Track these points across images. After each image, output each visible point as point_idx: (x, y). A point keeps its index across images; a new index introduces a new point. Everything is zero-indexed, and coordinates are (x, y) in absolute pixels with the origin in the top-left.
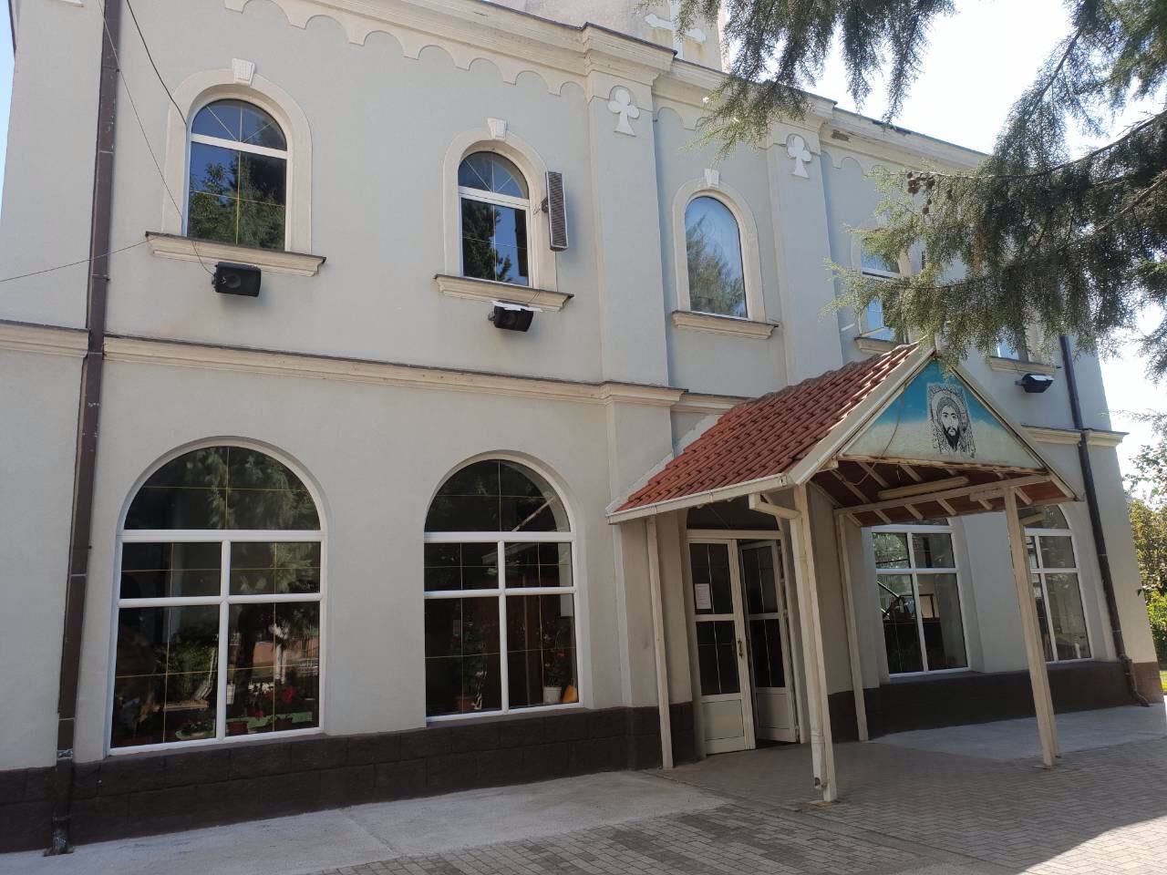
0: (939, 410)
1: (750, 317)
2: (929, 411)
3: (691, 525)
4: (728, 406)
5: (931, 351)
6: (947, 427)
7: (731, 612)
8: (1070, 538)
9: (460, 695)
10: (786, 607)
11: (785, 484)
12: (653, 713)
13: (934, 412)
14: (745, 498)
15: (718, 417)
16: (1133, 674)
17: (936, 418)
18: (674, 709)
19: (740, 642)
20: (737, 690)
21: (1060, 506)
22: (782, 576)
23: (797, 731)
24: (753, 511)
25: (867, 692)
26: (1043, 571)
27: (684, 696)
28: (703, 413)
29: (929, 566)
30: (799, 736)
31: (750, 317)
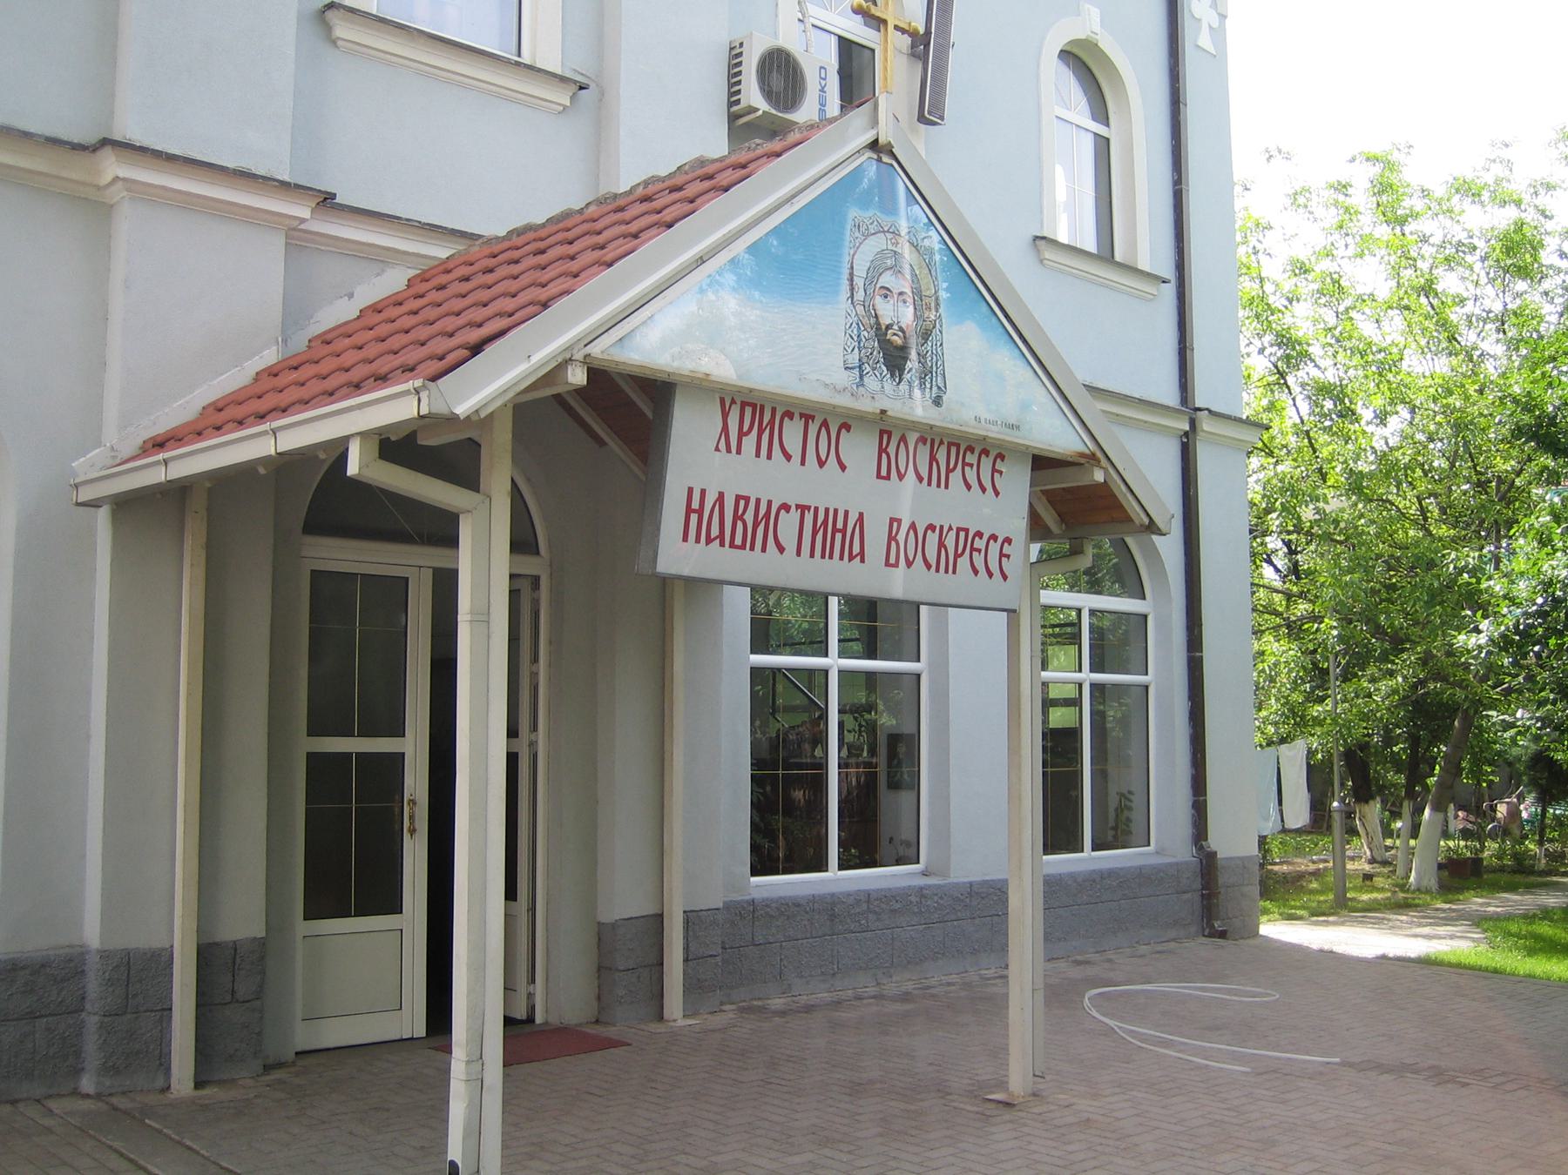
0: (871, 280)
1: (1187, 428)
2: (846, 276)
3: (316, 525)
4: (441, 251)
5: (869, 137)
6: (885, 321)
7: (401, 733)
8: (1145, 617)
9: (777, 813)
10: (534, 728)
11: (425, 411)
12: (160, 962)
13: (859, 282)
14: (339, 449)
15: (412, 273)
16: (1222, 879)
17: (860, 295)
18: (207, 955)
19: (413, 802)
20: (395, 907)
21: (1129, 540)
22: (535, 660)
23: (530, 996)
24: (355, 483)
25: (691, 918)
26: (1087, 676)
27: (243, 920)
28: (381, 258)
29: (871, 654)
30: (533, 1007)
31: (1187, 428)
